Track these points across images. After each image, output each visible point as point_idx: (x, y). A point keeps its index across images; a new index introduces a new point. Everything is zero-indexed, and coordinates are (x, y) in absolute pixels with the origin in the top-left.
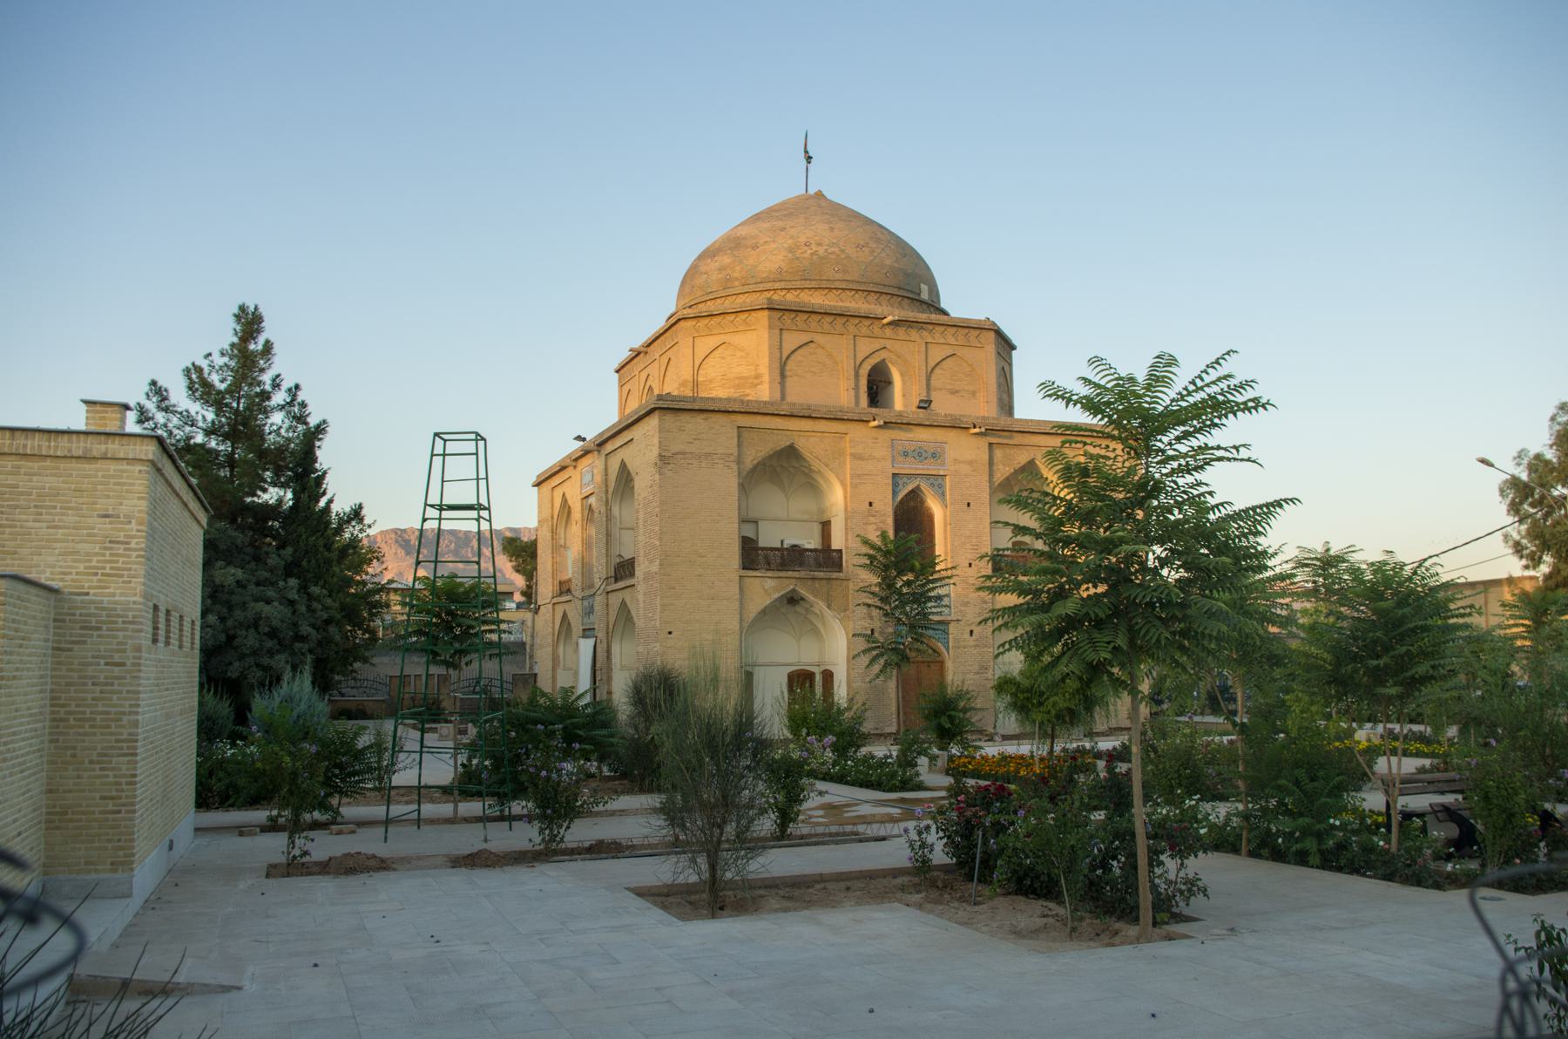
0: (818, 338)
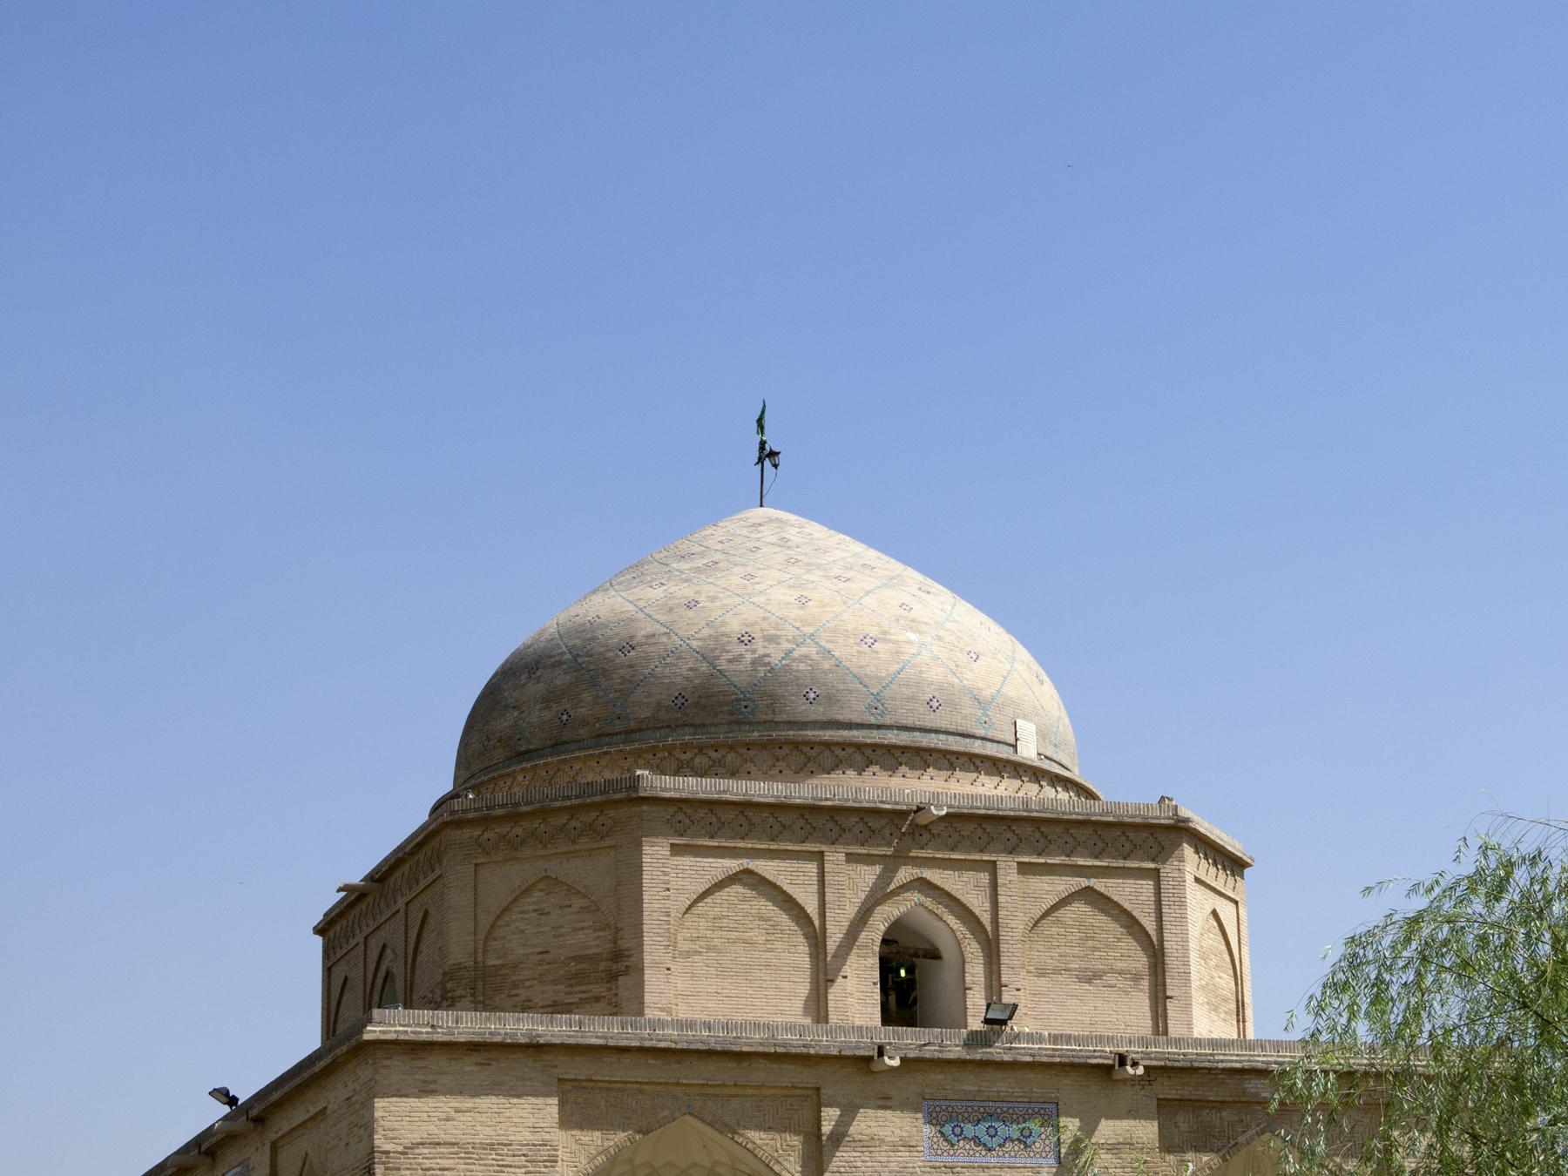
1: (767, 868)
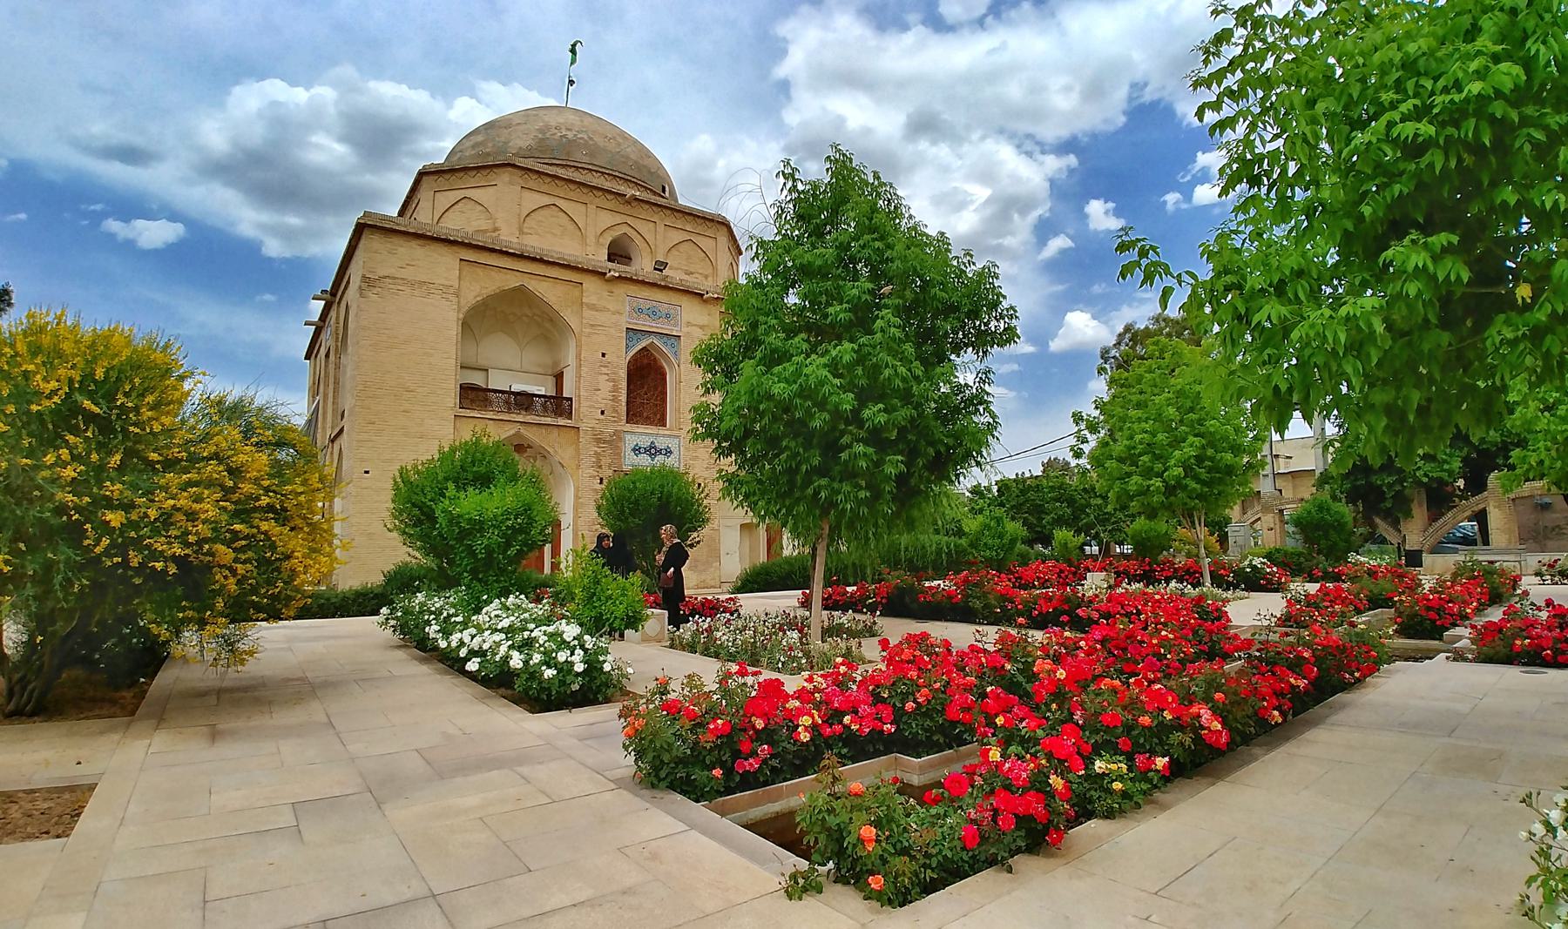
0: (560, 203)
1: (560, 203)
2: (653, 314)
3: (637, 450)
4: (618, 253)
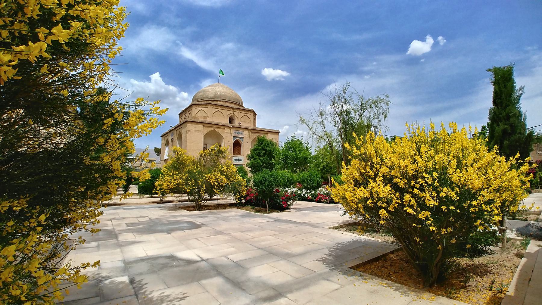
2: (238, 133)
3: (235, 160)
4: (231, 120)
